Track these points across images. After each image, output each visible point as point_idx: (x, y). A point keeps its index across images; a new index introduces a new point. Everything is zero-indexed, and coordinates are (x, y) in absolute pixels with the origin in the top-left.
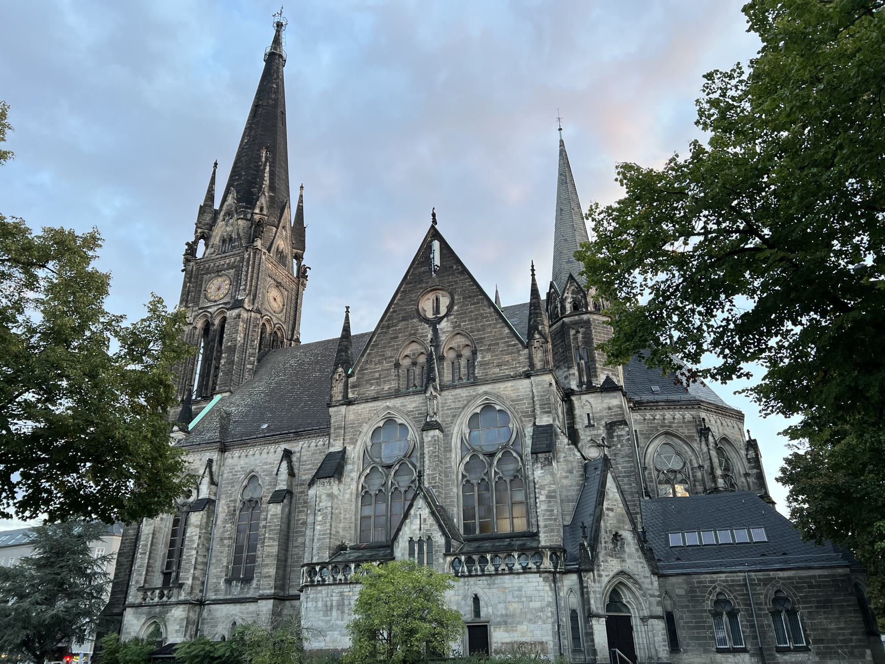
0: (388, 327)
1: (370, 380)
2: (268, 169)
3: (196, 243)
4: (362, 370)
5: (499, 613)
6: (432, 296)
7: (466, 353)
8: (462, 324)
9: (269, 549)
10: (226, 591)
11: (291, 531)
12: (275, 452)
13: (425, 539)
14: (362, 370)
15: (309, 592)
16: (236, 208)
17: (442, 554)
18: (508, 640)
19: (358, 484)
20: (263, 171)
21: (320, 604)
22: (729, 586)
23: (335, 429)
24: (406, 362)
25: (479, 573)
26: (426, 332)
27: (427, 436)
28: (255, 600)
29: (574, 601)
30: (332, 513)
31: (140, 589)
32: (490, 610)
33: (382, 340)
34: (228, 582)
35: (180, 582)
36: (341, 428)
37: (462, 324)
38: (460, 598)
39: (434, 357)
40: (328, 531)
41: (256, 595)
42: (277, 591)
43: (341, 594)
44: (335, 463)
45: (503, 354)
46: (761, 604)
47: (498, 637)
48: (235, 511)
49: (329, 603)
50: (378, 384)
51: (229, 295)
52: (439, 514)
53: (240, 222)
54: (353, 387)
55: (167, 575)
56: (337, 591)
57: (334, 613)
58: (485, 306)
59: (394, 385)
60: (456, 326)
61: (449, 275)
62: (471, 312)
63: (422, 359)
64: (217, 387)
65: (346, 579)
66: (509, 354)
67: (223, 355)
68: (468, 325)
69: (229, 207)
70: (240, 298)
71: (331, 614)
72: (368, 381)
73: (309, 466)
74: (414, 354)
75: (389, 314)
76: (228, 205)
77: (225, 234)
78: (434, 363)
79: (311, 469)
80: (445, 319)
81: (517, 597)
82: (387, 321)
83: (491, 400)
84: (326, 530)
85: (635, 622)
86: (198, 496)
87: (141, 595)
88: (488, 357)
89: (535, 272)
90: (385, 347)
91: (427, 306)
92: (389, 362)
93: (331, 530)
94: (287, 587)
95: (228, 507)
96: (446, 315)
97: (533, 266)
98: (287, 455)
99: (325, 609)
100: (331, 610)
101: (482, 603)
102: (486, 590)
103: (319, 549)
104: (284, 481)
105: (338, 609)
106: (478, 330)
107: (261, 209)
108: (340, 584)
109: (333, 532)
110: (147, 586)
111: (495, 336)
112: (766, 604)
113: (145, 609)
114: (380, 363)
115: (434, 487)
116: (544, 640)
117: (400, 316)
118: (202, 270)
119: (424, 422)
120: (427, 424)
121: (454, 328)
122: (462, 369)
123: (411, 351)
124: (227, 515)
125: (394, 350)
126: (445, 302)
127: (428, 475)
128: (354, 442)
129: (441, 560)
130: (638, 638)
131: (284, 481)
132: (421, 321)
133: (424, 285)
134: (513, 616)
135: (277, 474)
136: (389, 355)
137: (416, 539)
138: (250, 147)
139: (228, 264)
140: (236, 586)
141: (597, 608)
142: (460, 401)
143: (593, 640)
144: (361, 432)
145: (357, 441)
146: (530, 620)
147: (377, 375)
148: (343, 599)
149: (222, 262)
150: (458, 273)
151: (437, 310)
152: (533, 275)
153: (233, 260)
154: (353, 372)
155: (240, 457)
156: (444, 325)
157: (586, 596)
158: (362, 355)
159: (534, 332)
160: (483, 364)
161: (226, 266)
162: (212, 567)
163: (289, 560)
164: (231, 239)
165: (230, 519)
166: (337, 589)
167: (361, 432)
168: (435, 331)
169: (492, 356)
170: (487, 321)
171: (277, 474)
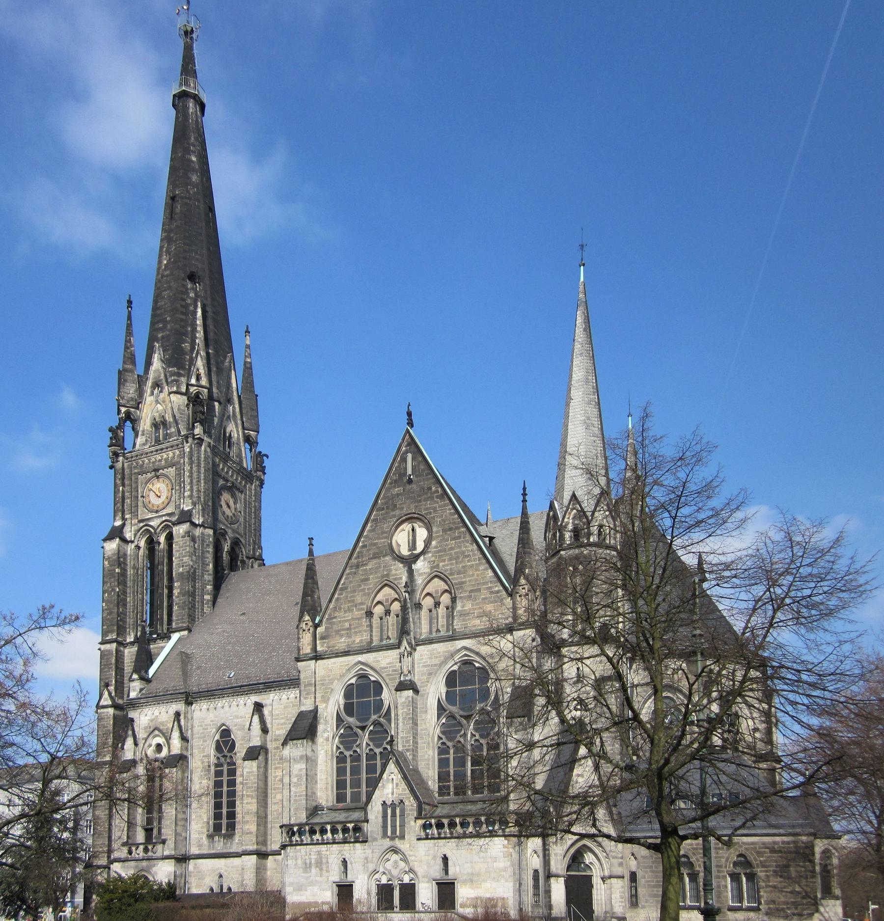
0: (358, 566)
1: (339, 631)
2: (199, 311)
3: (121, 426)
4: (330, 618)
5: (465, 872)
6: (407, 527)
7: (445, 599)
8: (441, 564)
9: (249, 807)
10: (209, 846)
11: (269, 787)
12: (245, 704)
13: (397, 803)
14: (330, 618)
15: (288, 851)
16: (166, 376)
17: (413, 818)
18: (473, 896)
19: (332, 745)
20: (195, 313)
21: (299, 862)
22: (694, 849)
23: (305, 686)
24: (379, 610)
25: (448, 835)
26: (401, 574)
27: (400, 697)
28: (238, 855)
29: (536, 862)
30: (307, 775)
31: (124, 844)
32: (458, 869)
33: (351, 582)
34: (210, 837)
35: (163, 838)
36: (311, 684)
37: (441, 564)
38: (430, 858)
39: (409, 605)
40: (304, 793)
41: (240, 850)
42: (259, 847)
43: (319, 853)
44: (306, 723)
45: (485, 603)
46: (721, 866)
47: (463, 893)
48: (209, 766)
49: (308, 861)
50: (349, 636)
51: (172, 504)
52: (412, 778)
53: (173, 397)
54: (322, 638)
55: (148, 831)
56: (315, 850)
57: (314, 870)
58: (467, 542)
59: (365, 637)
60: (434, 566)
61: (426, 500)
62: (452, 549)
63: (396, 606)
64: (174, 624)
65: (323, 839)
66: (491, 602)
67: (176, 584)
68: (447, 565)
69: (156, 375)
70: (186, 509)
71: (310, 870)
72: (338, 632)
73: (283, 721)
74: (387, 600)
75: (358, 550)
76: (155, 371)
77: (156, 415)
78: (408, 613)
79: (285, 724)
80: (422, 558)
81: (483, 858)
82: (356, 559)
83: (469, 656)
84: (302, 792)
85: (596, 881)
86: (169, 752)
87: (125, 850)
88: (468, 606)
89: (527, 498)
90: (354, 591)
91: (401, 539)
92: (359, 610)
93: (307, 791)
94: (269, 843)
95: (203, 763)
96: (423, 553)
97: (524, 489)
98: (258, 707)
99: (304, 866)
100: (310, 867)
101: (450, 863)
102: (454, 851)
103: (296, 809)
104: (257, 736)
105: (317, 867)
106: (459, 573)
107: (198, 378)
108: (317, 844)
109: (309, 794)
110: (130, 841)
111: (477, 580)
112: (726, 867)
113: (133, 863)
114: (349, 610)
115: (407, 750)
116: (505, 896)
117: (371, 552)
118: (135, 467)
119: (397, 681)
120: (401, 683)
121: (432, 568)
122: (440, 619)
123: (384, 596)
124: (202, 771)
125: (365, 595)
126: (422, 533)
127: (402, 738)
128: (326, 700)
129: (412, 823)
130: (597, 895)
131: (257, 736)
132: (394, 559)
133: (397, 512)
134: (478, 874)
135: (249, 729)
136: (360, 601)
137: (389, 803)
138: (172, 274)
139: (166, 460)
140: (219, 841)
141: (557, 869)
142: (437, 657)
143: (550, 897)
144: (332, 690)
145: (329, 699)
146: (494, 878)
147: (347, 625)
148: (321, 858)
149: (158, 457)
150: (437, 497)
151: (413, 545)
152: (524, 501)
153: (171, 454)
154: (321, 621)
155: (208, 709)
156: (421, 566)
157: (547, 858)
158: (330, 601)
159: (520, 577)
160: (463, 614)
161: (163, 462)
162: (193, 823)
163: (269, 817)
164: (164, 423)
165: (206, 775)
166: (315, 848)
167: (332, 690)
168: (411, 572)
169: (473, 605)
170: (469, 561)
171: (249, 729)
